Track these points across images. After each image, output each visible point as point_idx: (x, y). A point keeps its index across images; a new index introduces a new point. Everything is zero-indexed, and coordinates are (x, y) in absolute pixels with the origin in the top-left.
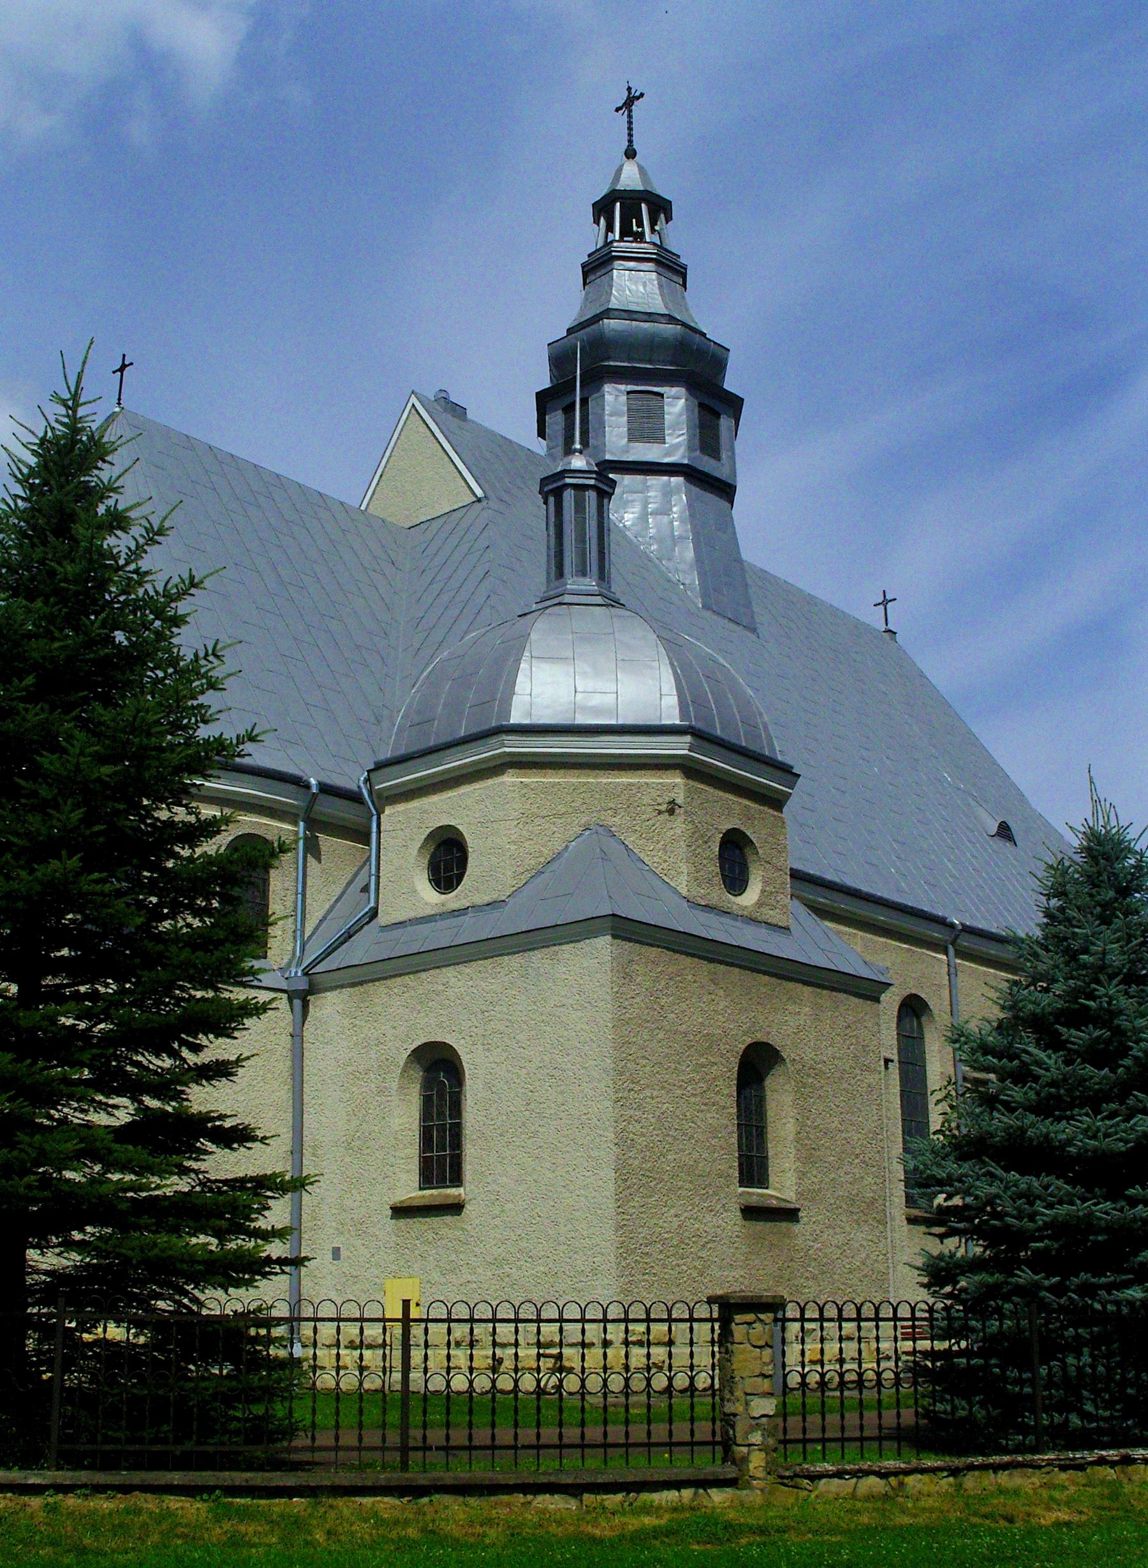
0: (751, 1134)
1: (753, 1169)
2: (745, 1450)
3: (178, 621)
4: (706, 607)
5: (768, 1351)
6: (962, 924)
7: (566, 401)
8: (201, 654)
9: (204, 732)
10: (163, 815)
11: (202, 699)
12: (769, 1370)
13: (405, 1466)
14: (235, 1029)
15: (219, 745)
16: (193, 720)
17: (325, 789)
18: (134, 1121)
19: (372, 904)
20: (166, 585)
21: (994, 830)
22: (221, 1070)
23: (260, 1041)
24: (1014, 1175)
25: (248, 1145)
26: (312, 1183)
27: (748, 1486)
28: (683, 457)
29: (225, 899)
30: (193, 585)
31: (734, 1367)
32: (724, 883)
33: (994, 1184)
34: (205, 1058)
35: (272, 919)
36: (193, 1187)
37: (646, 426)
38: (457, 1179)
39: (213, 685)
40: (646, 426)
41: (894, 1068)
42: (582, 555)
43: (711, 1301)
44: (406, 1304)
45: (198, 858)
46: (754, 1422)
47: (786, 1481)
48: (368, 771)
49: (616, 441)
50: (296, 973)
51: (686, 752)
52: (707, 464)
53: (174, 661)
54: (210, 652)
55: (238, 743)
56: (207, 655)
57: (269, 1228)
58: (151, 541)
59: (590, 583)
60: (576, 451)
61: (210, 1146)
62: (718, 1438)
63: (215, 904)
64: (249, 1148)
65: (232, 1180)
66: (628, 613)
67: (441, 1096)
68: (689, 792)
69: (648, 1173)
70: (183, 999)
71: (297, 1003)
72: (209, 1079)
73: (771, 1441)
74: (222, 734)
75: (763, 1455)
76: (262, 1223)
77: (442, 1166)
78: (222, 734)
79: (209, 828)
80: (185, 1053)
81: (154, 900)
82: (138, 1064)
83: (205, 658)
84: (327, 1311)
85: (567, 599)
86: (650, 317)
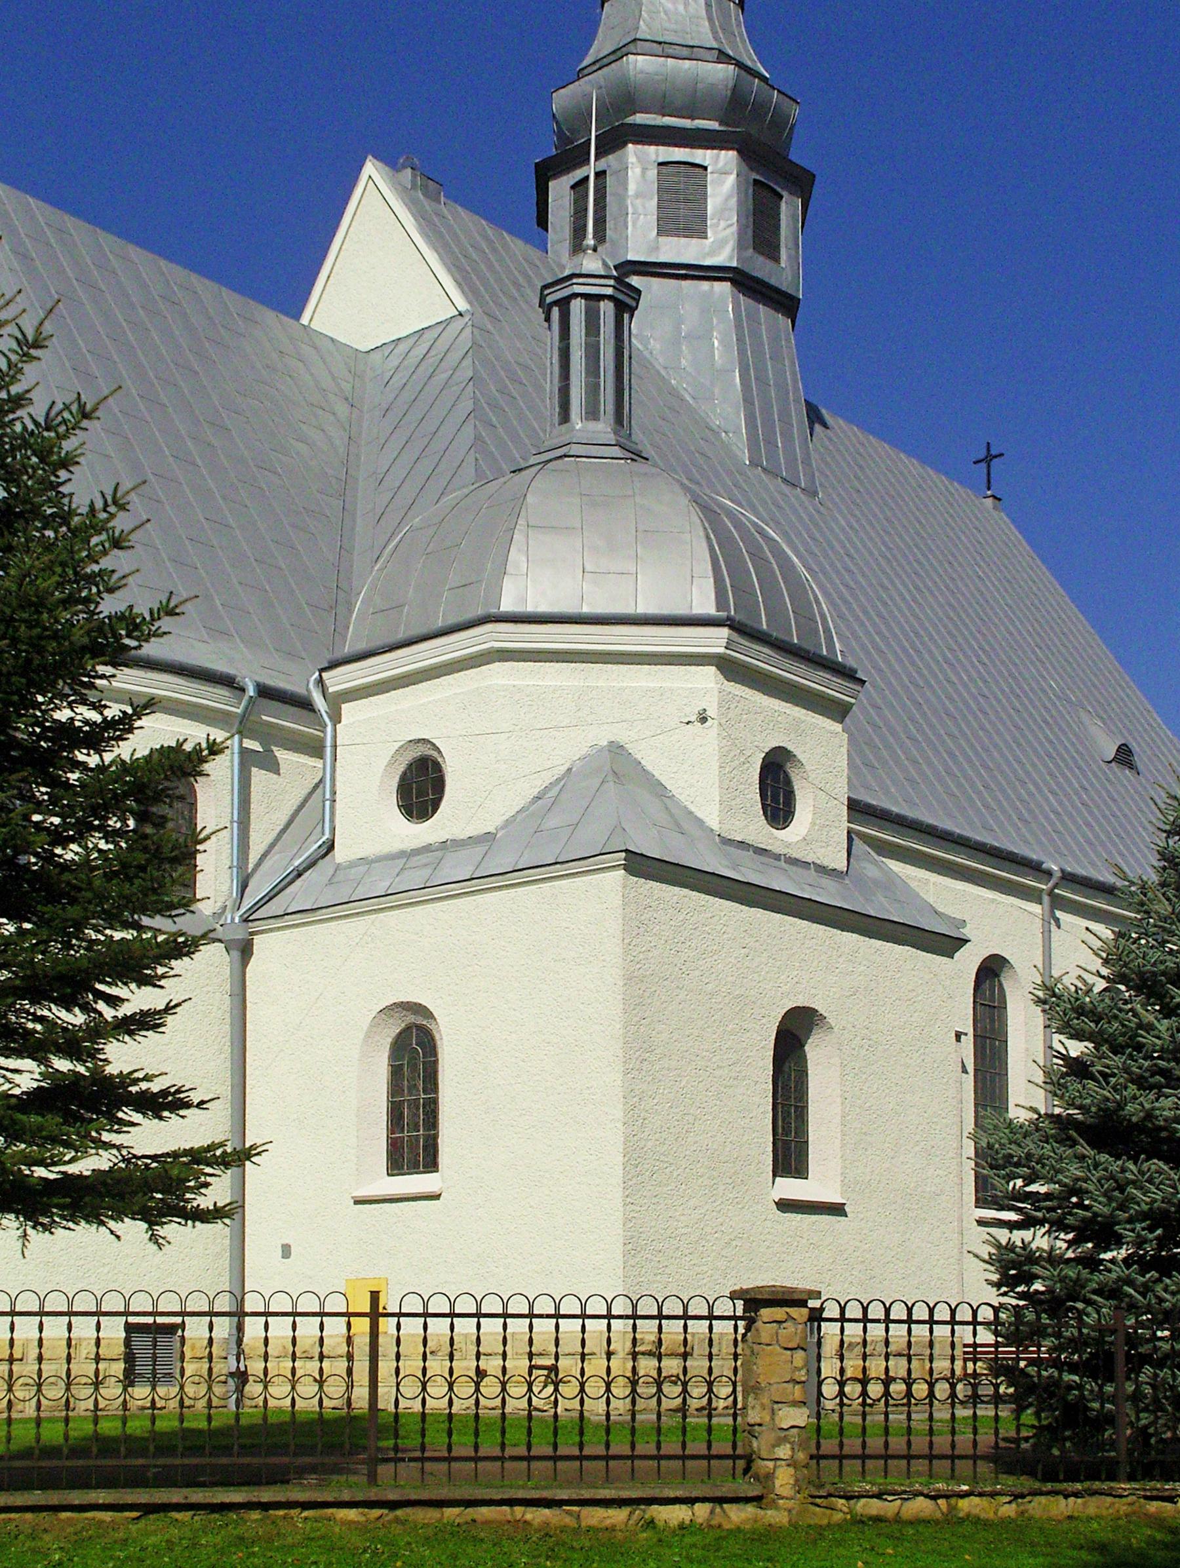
0: (789, 1113)
1: (790, 1157)
2: (771, 1464)
3: (67, 463)
4: (755, 463)
5: (799, 1356)
6: (1062, 871)
7: (578, 174)
8: (99, 504)
9: (109, 606)
10: (63, 715)
11: (106, 563)
12: (802, 1375)
13: (373, 1478)
14: (163, 976)
15: (131, 623)
16: (94, 590)
17: (266, 692)
18: (39, 1088)
19: (327, 836)
20: (48, 414)
21: (1111, 753)
22: (146, 1022)
23: (197, 979)
24: (1103, 1157)
25: (182, 1112)
26: (258, 1154)
27: (773, 1504)
28: (731, 258)
29: (141, 818)
30: (86, 416)
31: (759, 1371)
32: (765, 813)
33: (1076, 1165)
34: (126, 1010)
35: (202, 836)
36: (115, 1164)
37: (681, 209)
38: (431, 1164)
39: (117, 543)
40: (681, 209)
41: (968, 1042)
42: (593, 390)
43: (733, 1296)
44: (375, 1296)
45: (110, 766)
46: (783, 1434)
47: (818, 1501)
48: (322, 670)
49: (640, 235)
50: (233, 919)
51: (722, 650)
52: (761, 268)
53: (65, 517)
54: (110, 500)
55: (153, 620)
56: (106, 505)
57: (211, 1208)
58: (27, 357)
59: (603, 429)
60: (588, 247)
61: (136, 1117)
62: (739, 1451)
63: (131, 823)
64: (183, 1117)
65: (162, 1155)
66: (654, 470)
67: (413, 1067)
68: (725, 703)
69: (662, 1158)
70: (97, 942)
71: (236, 954)
72: (131, 1033)
73: (801, 1456)
74: (131, 607)
75: (791, 1470)
76: (204, 1201)
77: (413, 1147)
78: (131, 607)
79: (124, 726)
80: (101, 1006)
81: (56, 820)
82: (41, 1019)
83: (105, 510)
84: (281, 1304)
85: (575, 449)
86: (692, 52)
